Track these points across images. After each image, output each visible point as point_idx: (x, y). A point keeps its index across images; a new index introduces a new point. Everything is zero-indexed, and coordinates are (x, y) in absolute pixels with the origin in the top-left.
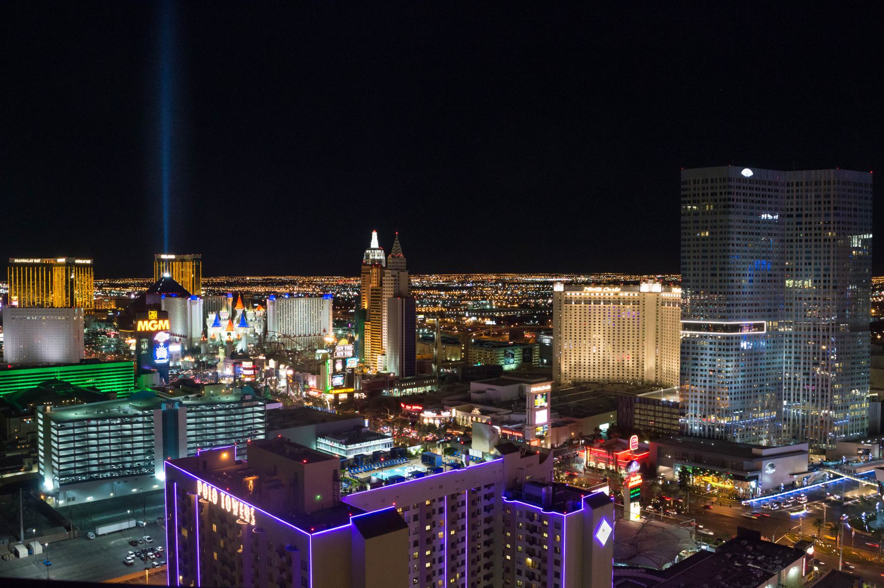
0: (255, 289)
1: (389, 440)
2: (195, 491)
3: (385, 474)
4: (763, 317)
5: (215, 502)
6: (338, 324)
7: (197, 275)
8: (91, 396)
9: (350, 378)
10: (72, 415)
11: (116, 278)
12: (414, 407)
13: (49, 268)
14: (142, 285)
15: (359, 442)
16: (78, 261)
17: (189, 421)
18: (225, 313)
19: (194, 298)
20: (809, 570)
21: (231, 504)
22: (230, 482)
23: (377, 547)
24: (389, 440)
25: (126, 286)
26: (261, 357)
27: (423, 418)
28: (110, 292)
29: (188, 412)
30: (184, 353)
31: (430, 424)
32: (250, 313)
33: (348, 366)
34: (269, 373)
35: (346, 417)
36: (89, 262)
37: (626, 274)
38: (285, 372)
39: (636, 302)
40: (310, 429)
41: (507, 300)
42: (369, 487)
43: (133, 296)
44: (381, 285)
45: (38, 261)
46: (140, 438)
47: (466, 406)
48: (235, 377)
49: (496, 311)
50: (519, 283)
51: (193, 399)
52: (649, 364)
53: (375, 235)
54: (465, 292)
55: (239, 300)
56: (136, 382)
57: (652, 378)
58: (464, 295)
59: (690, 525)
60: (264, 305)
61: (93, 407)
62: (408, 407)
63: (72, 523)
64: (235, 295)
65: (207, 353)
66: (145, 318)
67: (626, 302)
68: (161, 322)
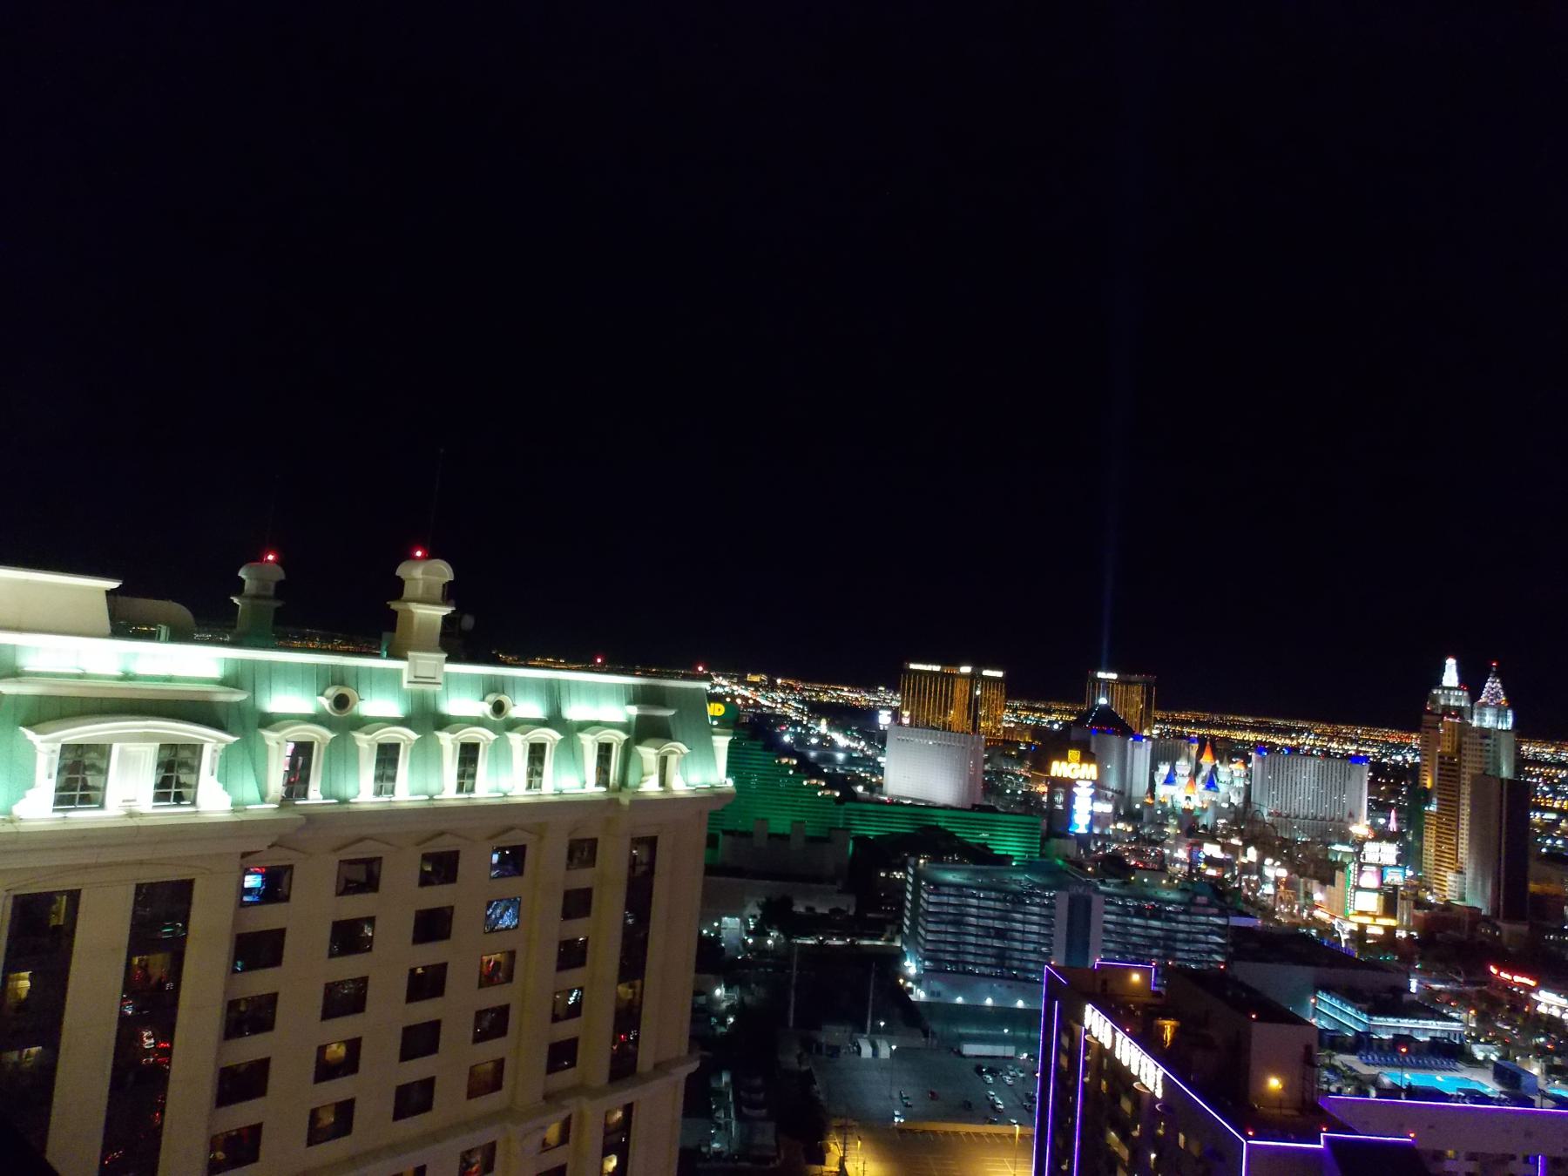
0: (1239, 736)
2: (1080, 1022)
3: (1409, 1077)
5: (1108, 1046)
6: (1378, 808)
7: (1148, 705)
8: (982, 856)
10: (950, 877)
11: (1037, 700)
12: (1517, 979)
13: (950, 678)
14: (1071, 713)
15: (1395, 1016)
16: (986, 673)
17: (1109, 917)
18: (1183, 767)
19: (1138, 738)
21: (1130, 1054)
22: (1137, 1020)
25: (1049, 712)
26: (1235, 841)
27: (1538, 1003)
28: (1027, 718)
29: (1107, 903)
30: (1117, 817)
31: (1550, 1017)
32: (1223, 771)
33: (1388, 879)
34: (1246, 869)
35: (1374, 966)
36: (999, 674)
38: (1275, 870)
40: (1304, 974)
42: (1373, 1093)
43: (1056, 726)
44: (1459, 751)
45: (937, 668)
46: (1035, 928)
51: (1116, 886)
53: (1451, 663)
55: (1208, 749)
56: (1042, 847)
60: (1247, 760)
61: (982, 872)
63: (935, 1027)
64: (1202, 741)
65: (1152, 822)
66: (1063, 757)
68: (1085, 765)
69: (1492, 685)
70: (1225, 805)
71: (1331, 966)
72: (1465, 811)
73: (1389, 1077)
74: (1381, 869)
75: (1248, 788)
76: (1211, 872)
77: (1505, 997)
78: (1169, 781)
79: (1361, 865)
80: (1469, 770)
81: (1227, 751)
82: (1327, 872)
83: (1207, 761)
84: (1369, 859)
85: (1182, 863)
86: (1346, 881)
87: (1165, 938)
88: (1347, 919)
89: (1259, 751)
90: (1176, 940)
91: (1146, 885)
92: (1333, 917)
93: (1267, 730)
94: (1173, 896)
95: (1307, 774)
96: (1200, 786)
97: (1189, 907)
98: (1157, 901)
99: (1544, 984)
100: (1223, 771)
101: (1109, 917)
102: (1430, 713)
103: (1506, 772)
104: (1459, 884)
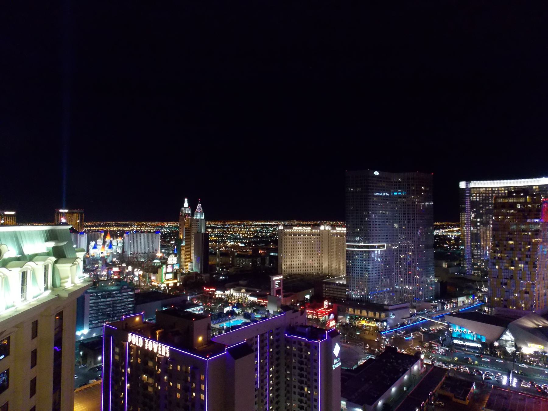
1: (201, 307)
2: (126, 340)
4: (385, 242)
6: (162, 247)
7: (81, 221)
9: (176, 274)
12: (211, 289)
16: (6, 213)
17: (91, 301)
18: (100, 242)
19: (82, 233)
20: (422, 366)
21: (152, 346)
23: (240, 363)
24: (201, 307)
29: (91, 296)
32: (114, 242)
33: (174, 268)
34: (128, 274)
36: (13, 213)
37: (125, 221)
38: (138, 272)
39: (318, 234)
41: (247, 234)
42: (224, 332)
47: (238, 288)
48: (108, 276)
49: (242, 239)
50: (252, 225)
52: (325, 265)
53: (186, 200)
54: (225, 230)
57: (327, 272)
58: (225, 231)
59: (361, 345)
62: (208, 289)
64: (106, 233)
67: (314, 234)
69: (199, 206)
70: (115, 253)
71: (166, 298)
72: (193, 244)
73: (225, 325)
74: (173, 265)
75: (123, 246)
76: (116, 277)
77: (208, 295)
78: (95, 247)
79: (167, 265)
80: (194, 232)
81: (114, 235)
82: (155, 270)
83: (108, 239)
84: (169, 263)
85: (104, 276)
86: (162, 271)
87: (113, 303)
88: (163, 283)
89: (127, 233)
90: (116, 303)
91: (103, 286)
92: (158, 283)
93: (121, 226)
94: (114, 288)
95: (142, 238)
96: (106, 248)
97: (120, 291)
98: (109, 291)
99: (217, 289)
100: (114, 242)
101: (91, 301)
102: (181, 216)
103: (203, 231)
104: (191, 266)
